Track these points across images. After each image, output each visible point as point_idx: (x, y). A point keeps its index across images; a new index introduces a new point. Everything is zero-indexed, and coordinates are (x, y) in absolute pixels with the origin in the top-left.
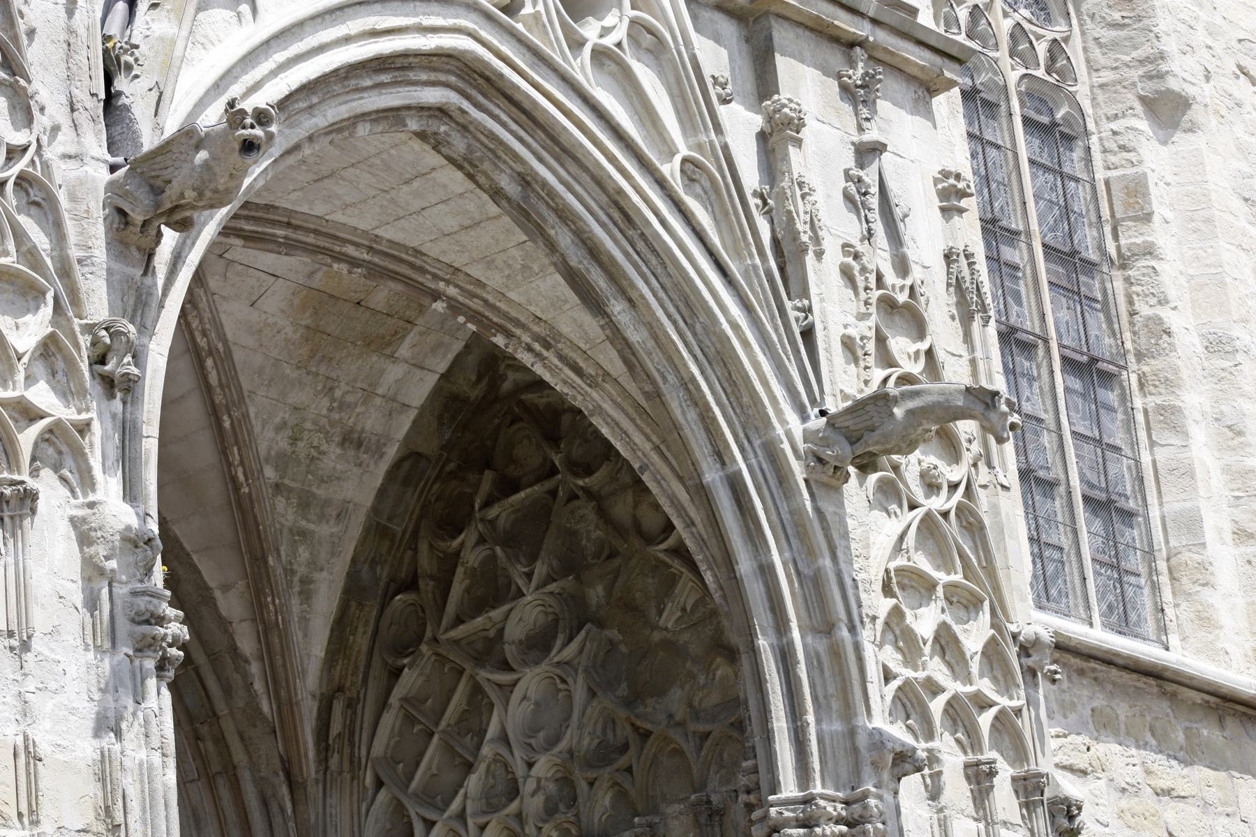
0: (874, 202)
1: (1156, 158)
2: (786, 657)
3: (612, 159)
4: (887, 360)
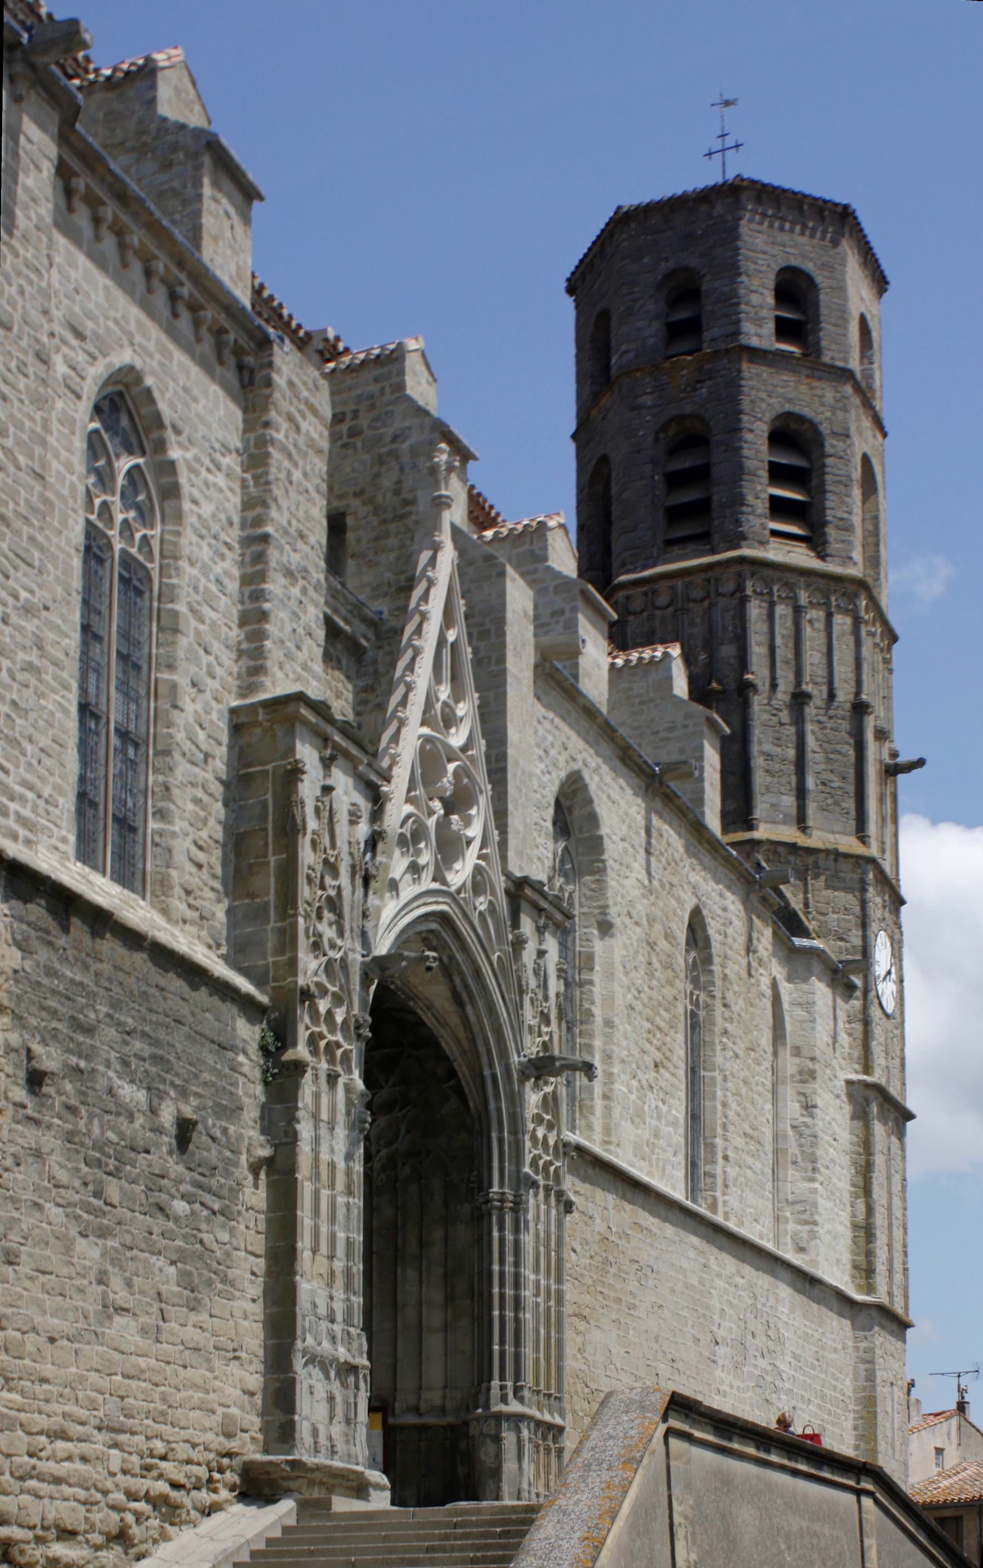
1: (598, 946)
2: (501, 1141)
4: (323, 887)
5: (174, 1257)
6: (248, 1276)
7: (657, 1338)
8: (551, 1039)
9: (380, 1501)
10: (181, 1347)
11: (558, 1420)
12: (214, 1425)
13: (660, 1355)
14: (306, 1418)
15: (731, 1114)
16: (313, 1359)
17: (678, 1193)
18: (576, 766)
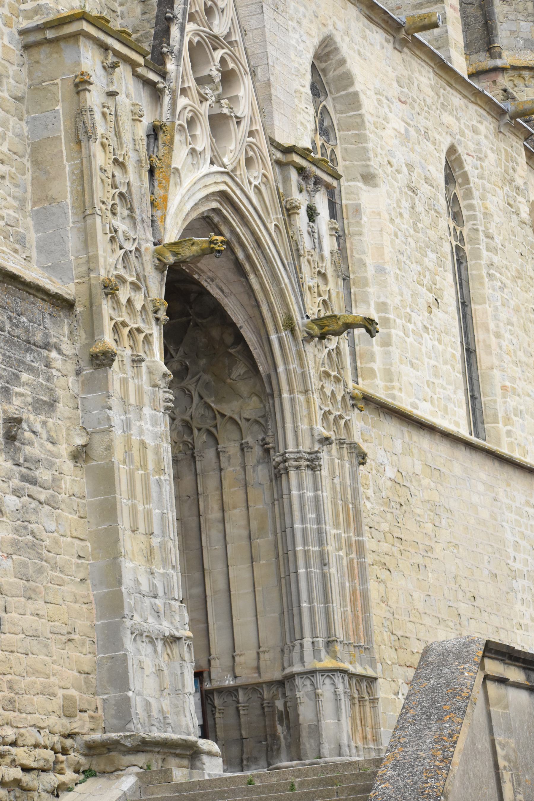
0: (316, 235)
3: (258, 226)
5: (10, 550)
6: (75, 560)
7: (455, 578)
8: (330, 298)
9: (213, 768)
10: (22, 636)
11: (370, 672)
12: (56, 708)
13: (460, 595)
14: (139, 694)
15: (504, 344)
16: (139, 635)
17: (463, 430)
18: (326, 32)
